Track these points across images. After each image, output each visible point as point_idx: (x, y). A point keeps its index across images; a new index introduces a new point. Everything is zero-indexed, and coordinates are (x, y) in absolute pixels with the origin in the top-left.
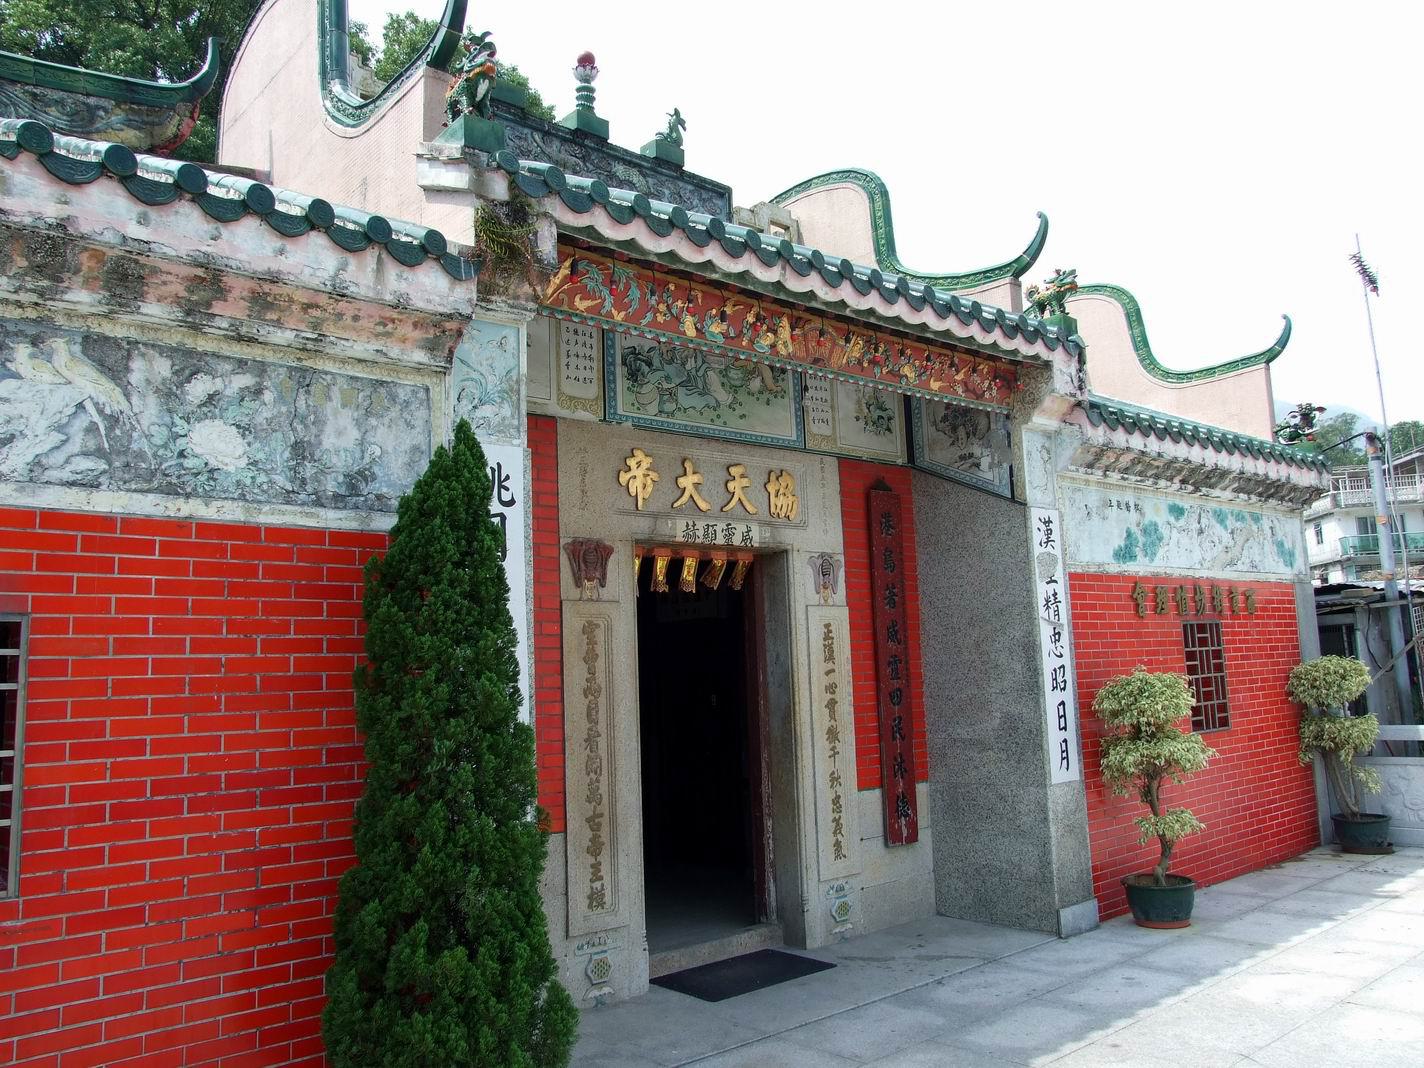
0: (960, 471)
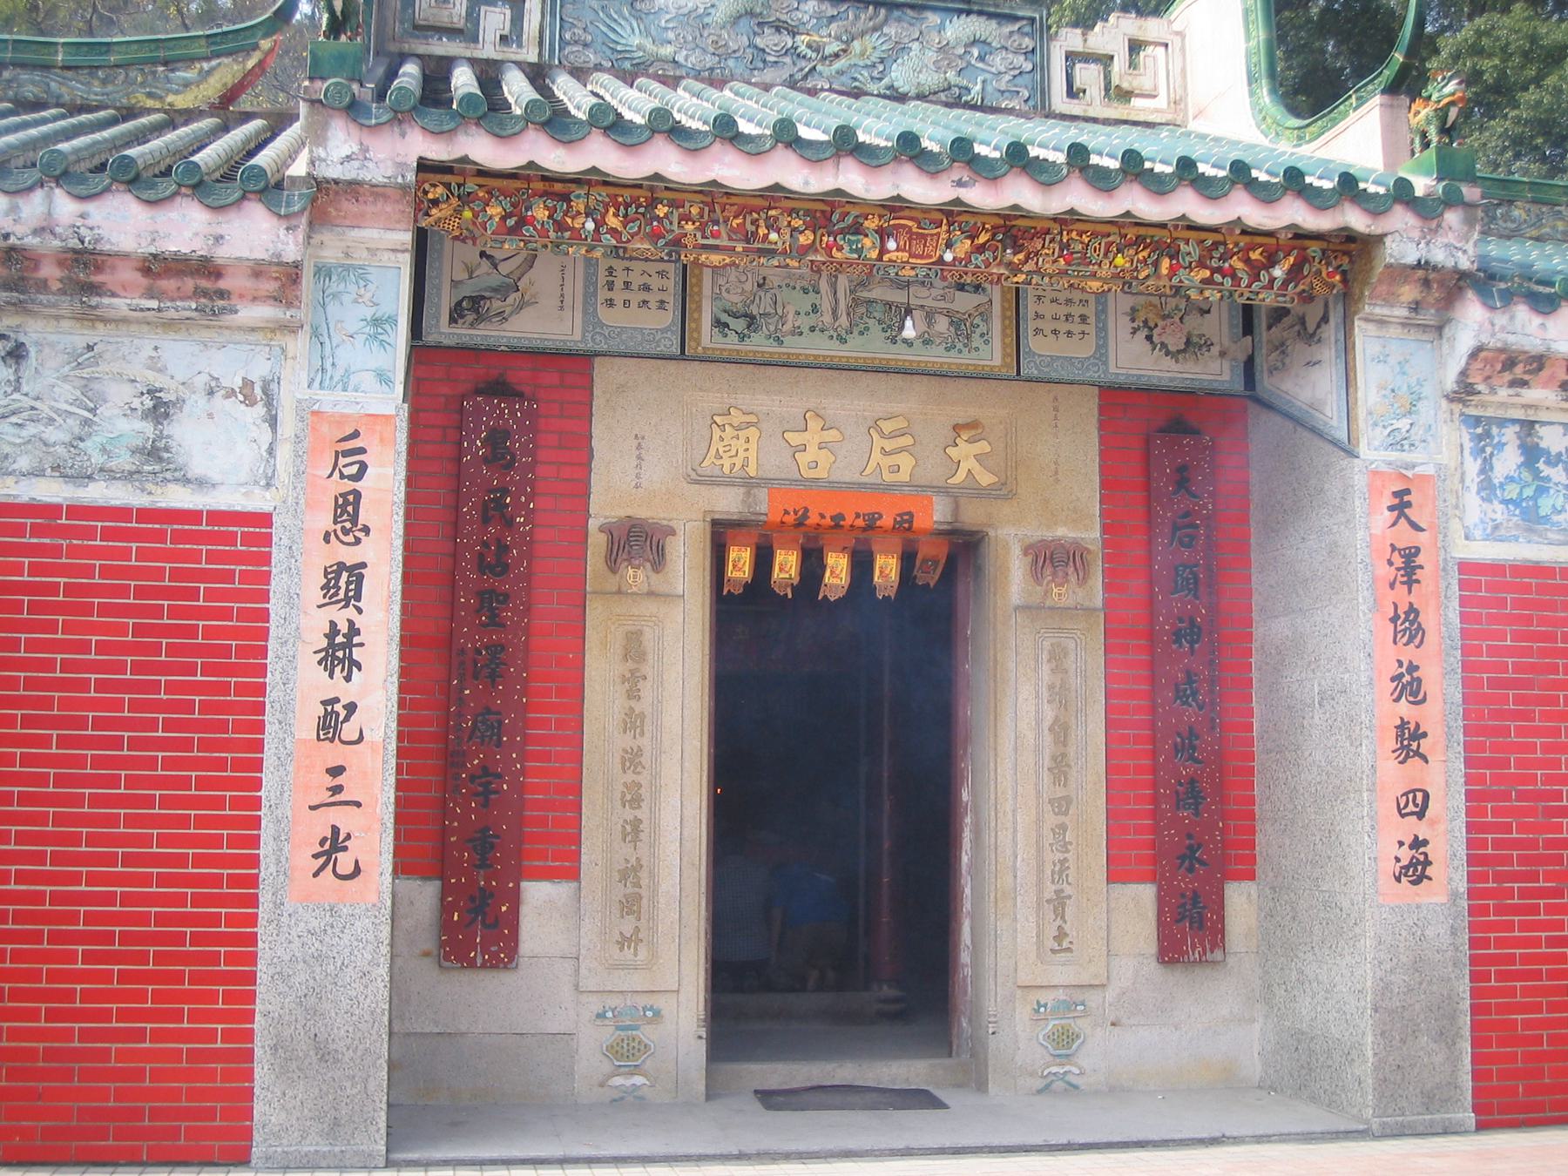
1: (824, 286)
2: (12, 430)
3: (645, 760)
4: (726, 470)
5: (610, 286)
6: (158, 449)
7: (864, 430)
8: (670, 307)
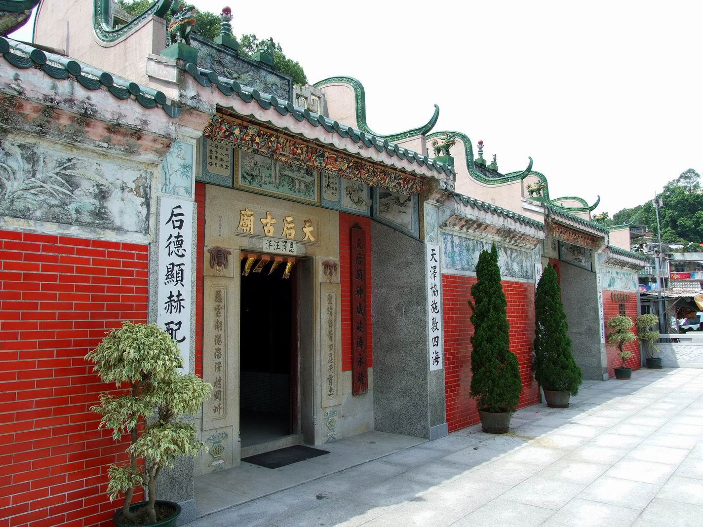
0: (576, 263)
1: (273, 168)
2: (31, 196)
3: (222, 339)
4: (245, 231)
5: (211, 157)
6: (102, 213)
7: (282, 220)
8: (229, 168)
